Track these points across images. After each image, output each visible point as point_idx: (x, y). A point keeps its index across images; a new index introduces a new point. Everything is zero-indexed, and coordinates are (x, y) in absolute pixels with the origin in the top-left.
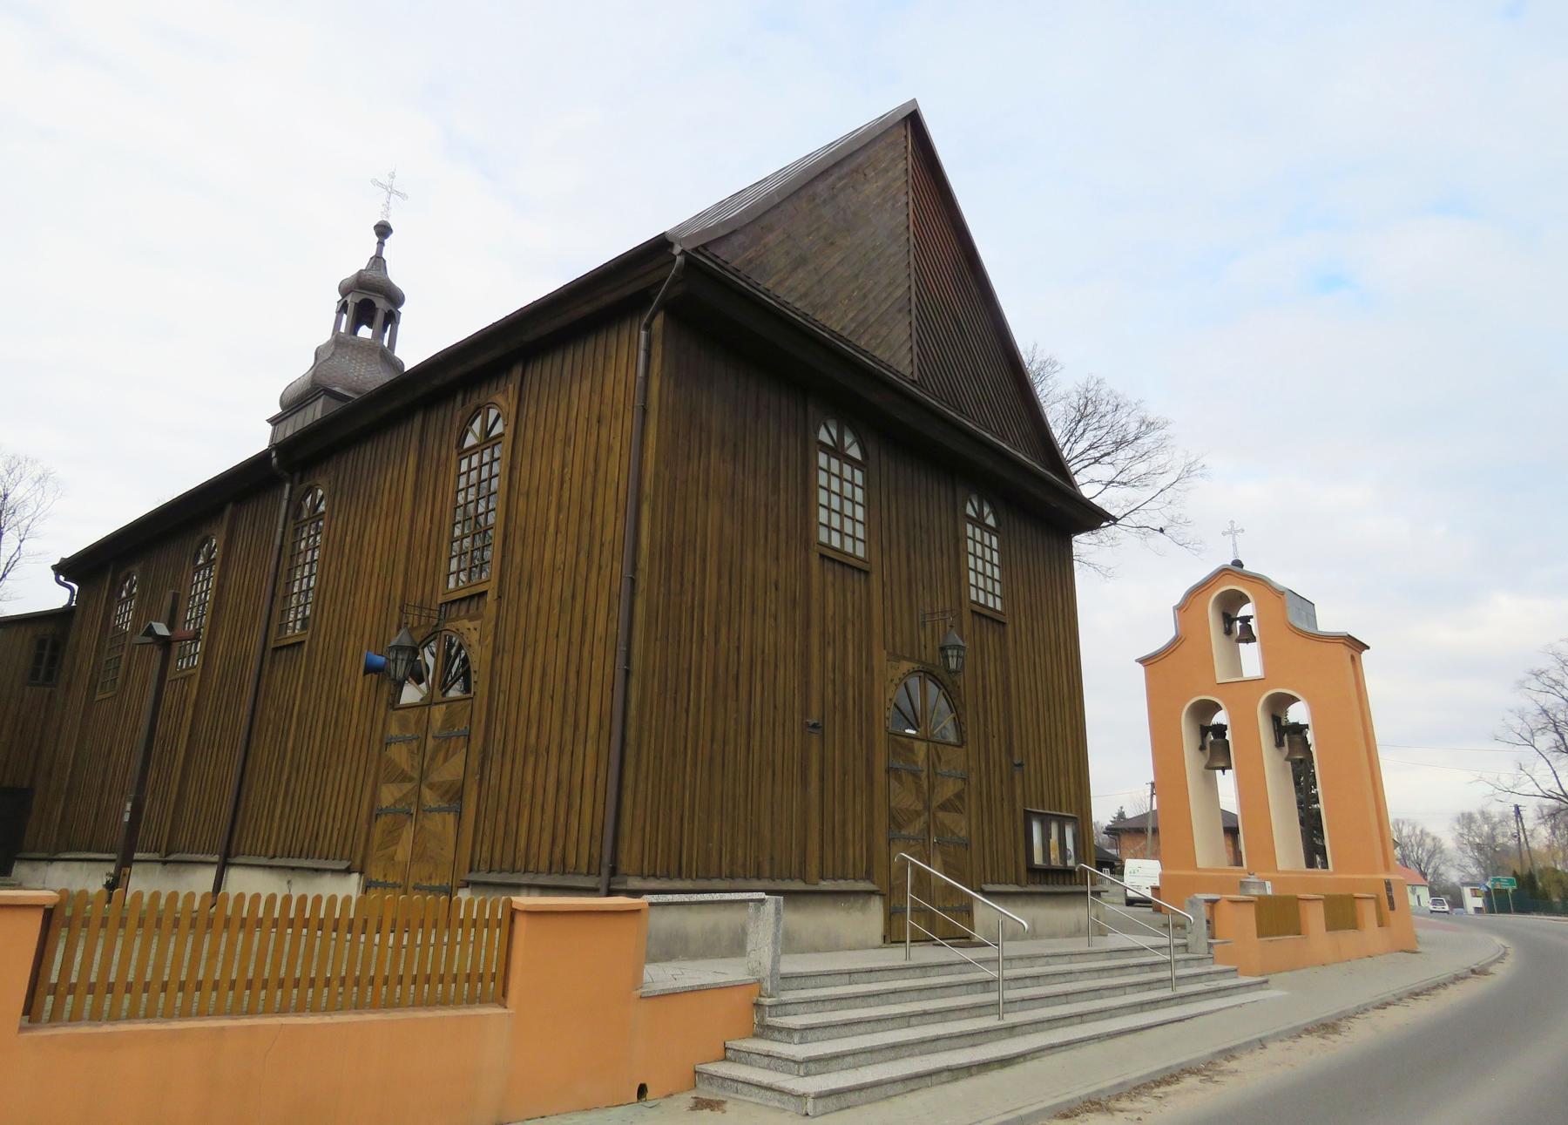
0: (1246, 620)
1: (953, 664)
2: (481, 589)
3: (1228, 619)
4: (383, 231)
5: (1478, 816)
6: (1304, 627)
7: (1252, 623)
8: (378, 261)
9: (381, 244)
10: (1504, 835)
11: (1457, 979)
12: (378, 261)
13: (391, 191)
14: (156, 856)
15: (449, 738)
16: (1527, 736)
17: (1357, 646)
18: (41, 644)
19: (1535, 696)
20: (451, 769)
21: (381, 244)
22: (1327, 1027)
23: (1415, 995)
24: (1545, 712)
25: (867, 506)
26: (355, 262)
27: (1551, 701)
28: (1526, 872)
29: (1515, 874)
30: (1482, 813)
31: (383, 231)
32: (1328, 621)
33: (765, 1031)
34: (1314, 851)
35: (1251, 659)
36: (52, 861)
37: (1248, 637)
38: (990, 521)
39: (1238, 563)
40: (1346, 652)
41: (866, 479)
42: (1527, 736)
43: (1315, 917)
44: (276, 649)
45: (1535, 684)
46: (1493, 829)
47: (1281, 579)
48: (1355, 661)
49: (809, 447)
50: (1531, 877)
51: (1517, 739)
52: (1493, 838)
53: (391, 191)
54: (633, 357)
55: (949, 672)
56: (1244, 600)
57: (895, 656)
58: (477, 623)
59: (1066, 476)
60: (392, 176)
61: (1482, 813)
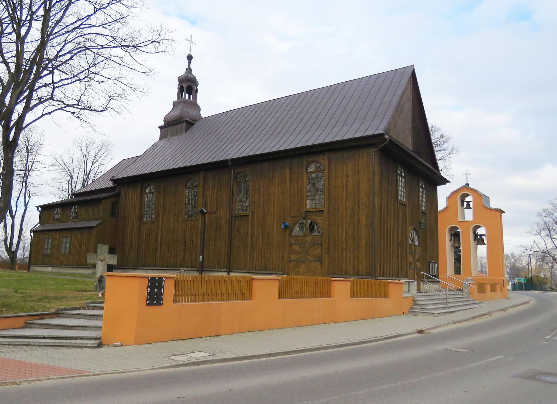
0: (468, 202)
1: (422, 227)
2: (323, 209)
3: (463, 202)
4: (190, 58)
5: (510, 255)
6: (488, 206)
7: (471, 203)
8: (189, 69)
9: (190, 63)
10: (519, 263)
11: (523, 304)
12: (189, 69)
13: (191, 42)
14: (195, 269)
15: (314, 244)
16: (538, 231)
17: (502, 212)
18: (113, 204)
19: (543, 217)
20: (318, 251)
21: (190, 63)
22: (503, 310)
23: (516, 306)
24: (546, 223)
25: (405, 188)
26: (182, 72)
27: (548, 220)
28: (530, 277)
29: (526, 277)
30: (512, 255)
31: (190, 58)
32: (493, 204)
33: (416, 304)
34: (458, 271)
35: (469, 215)
36: (136, 269)
37: (468, 207)
38: (403, 174)
39: (467, 184)
40: (498, 214)
41: (405, 181)
42: (538, 231)
43: (488, 287)
44: (235, 216)
45: (544, 214)
46: (515, 261)
47: (482, 190)
48: (501, 216)
49: (418, 187)
50: (531, 278)
51: (535, 233)
52: (515, 264)
53: (191, 42)
54: (370, 160)
55: (421, 229)
56: (468, 195)
57: (410, 225)
58: (321, 218)
59: (439, 172)
60: (191, 36)
61: (512, 255)
